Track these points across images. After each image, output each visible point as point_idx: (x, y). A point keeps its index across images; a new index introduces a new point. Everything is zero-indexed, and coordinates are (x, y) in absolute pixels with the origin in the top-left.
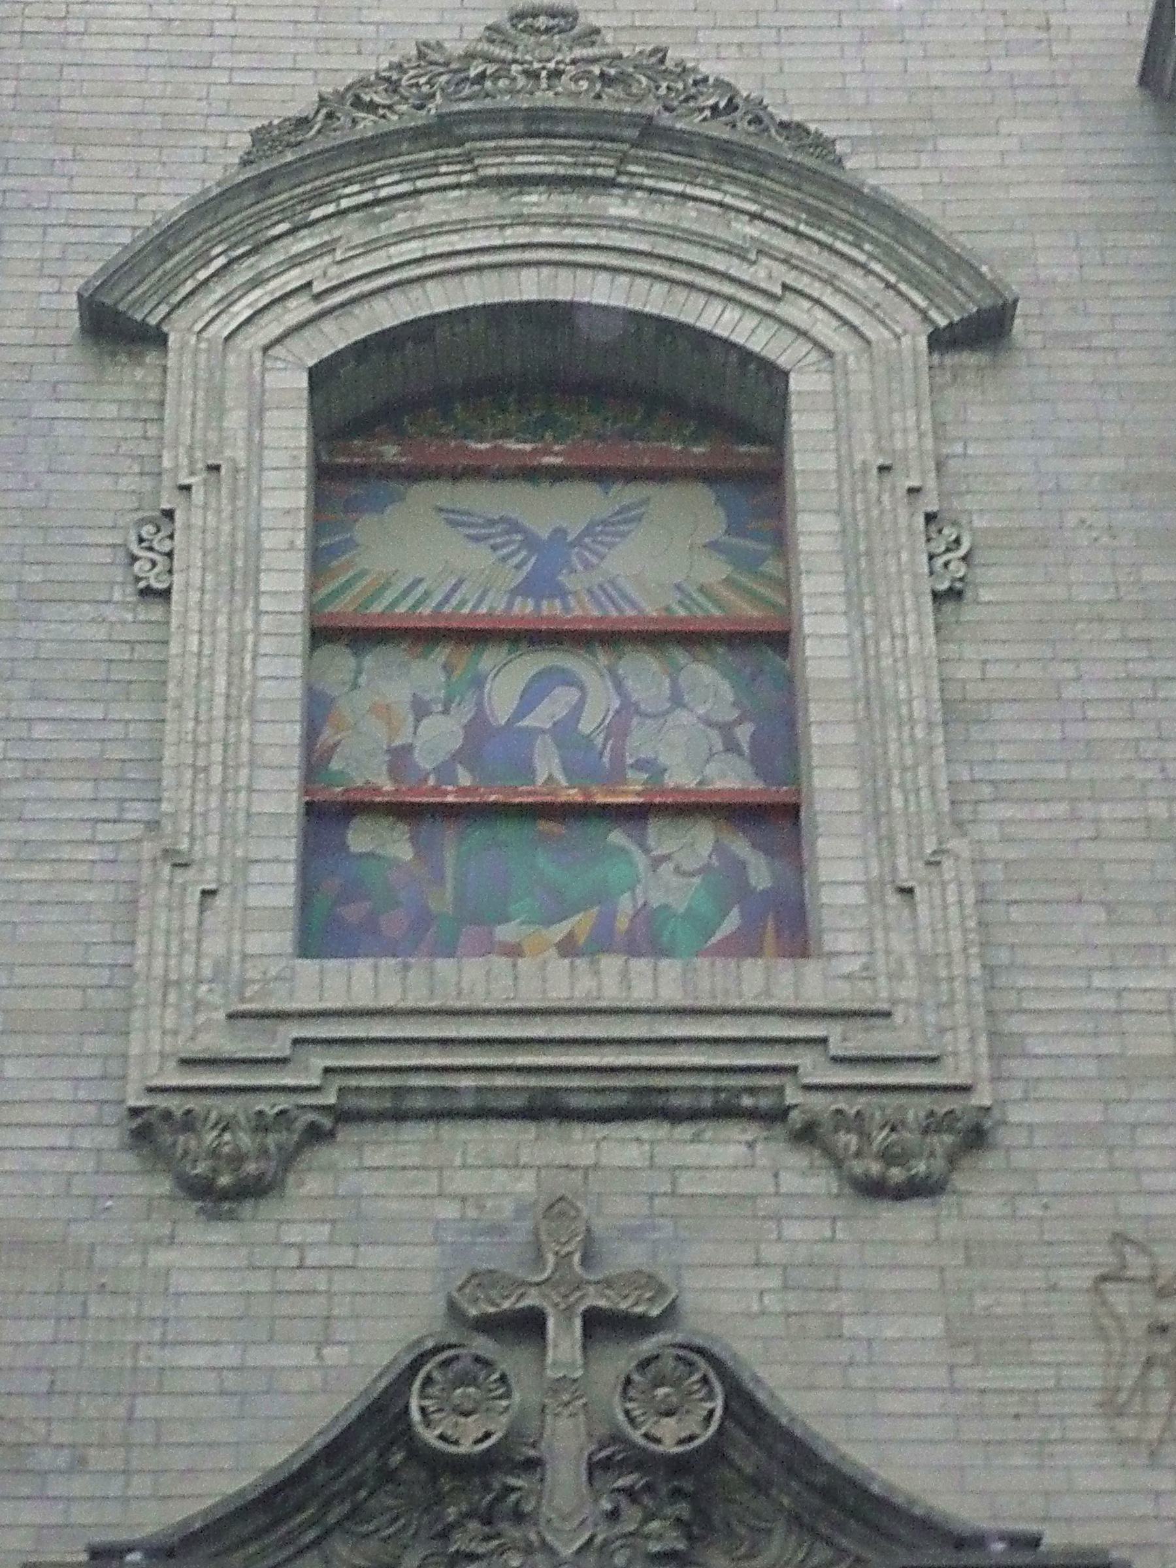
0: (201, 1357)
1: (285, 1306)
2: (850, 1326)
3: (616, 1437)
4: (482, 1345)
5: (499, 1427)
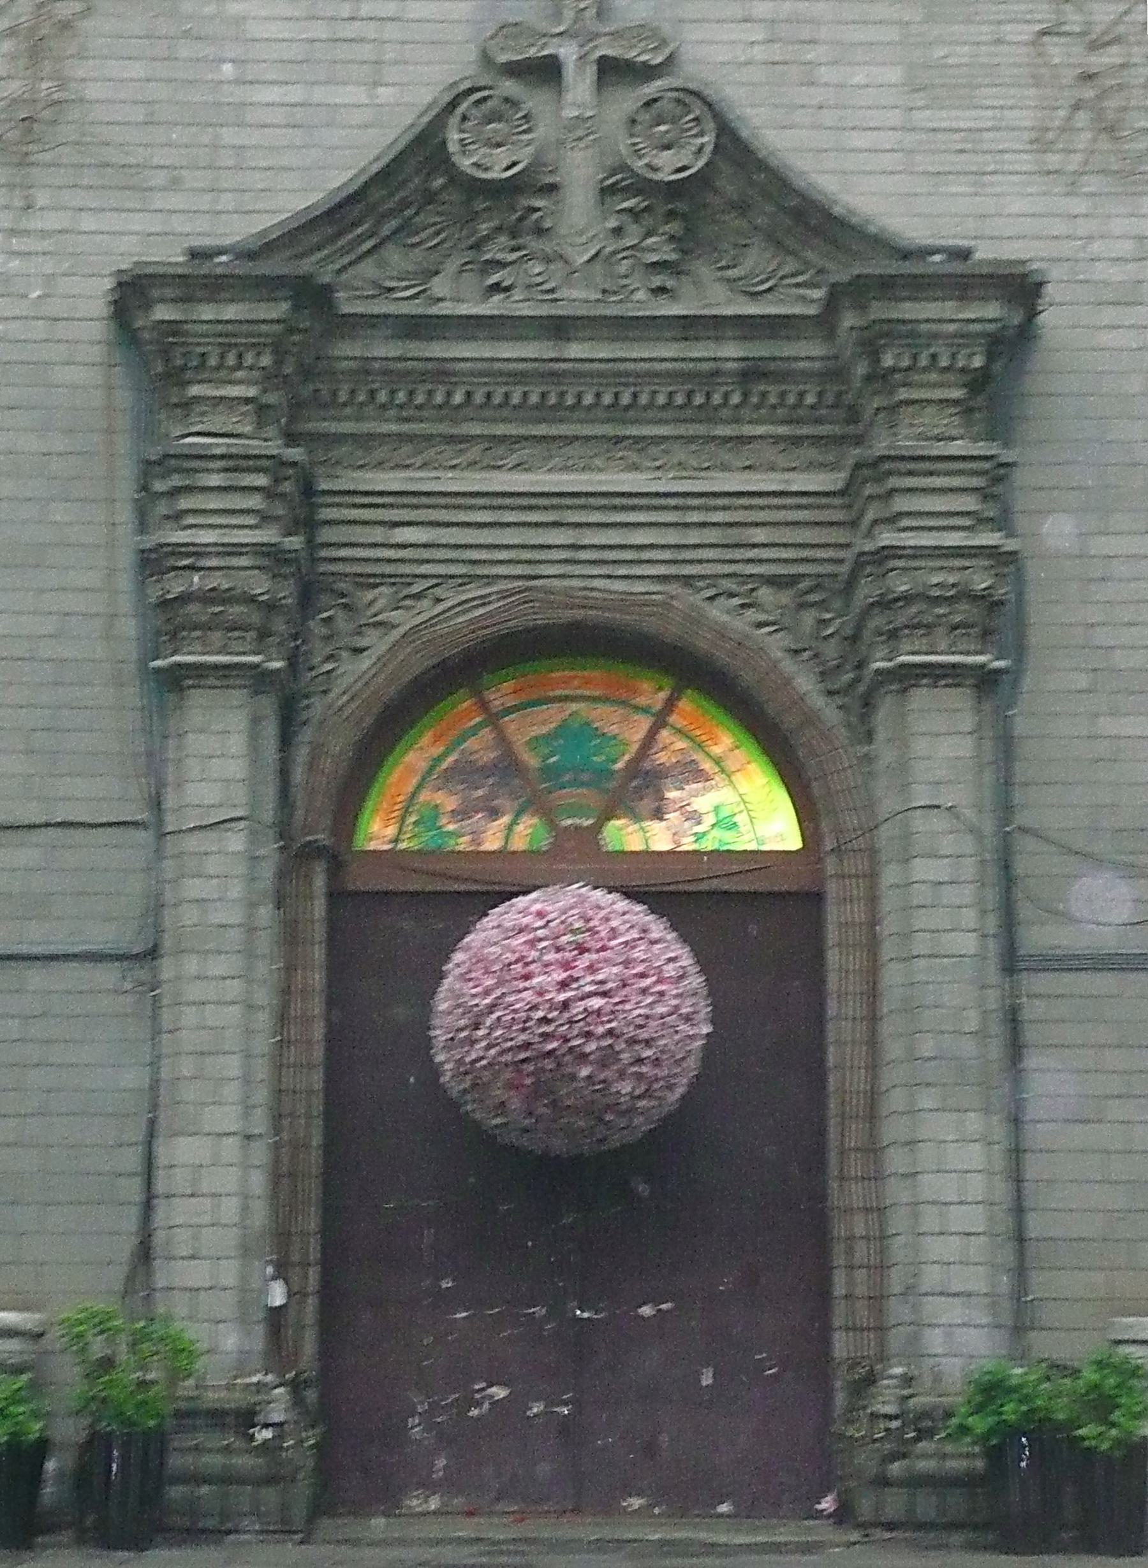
0: (272, 94)
1: (342, 52)
2: (825, 74)
3: (623, 167)
4: (509, 87)
5: (524, 157)
